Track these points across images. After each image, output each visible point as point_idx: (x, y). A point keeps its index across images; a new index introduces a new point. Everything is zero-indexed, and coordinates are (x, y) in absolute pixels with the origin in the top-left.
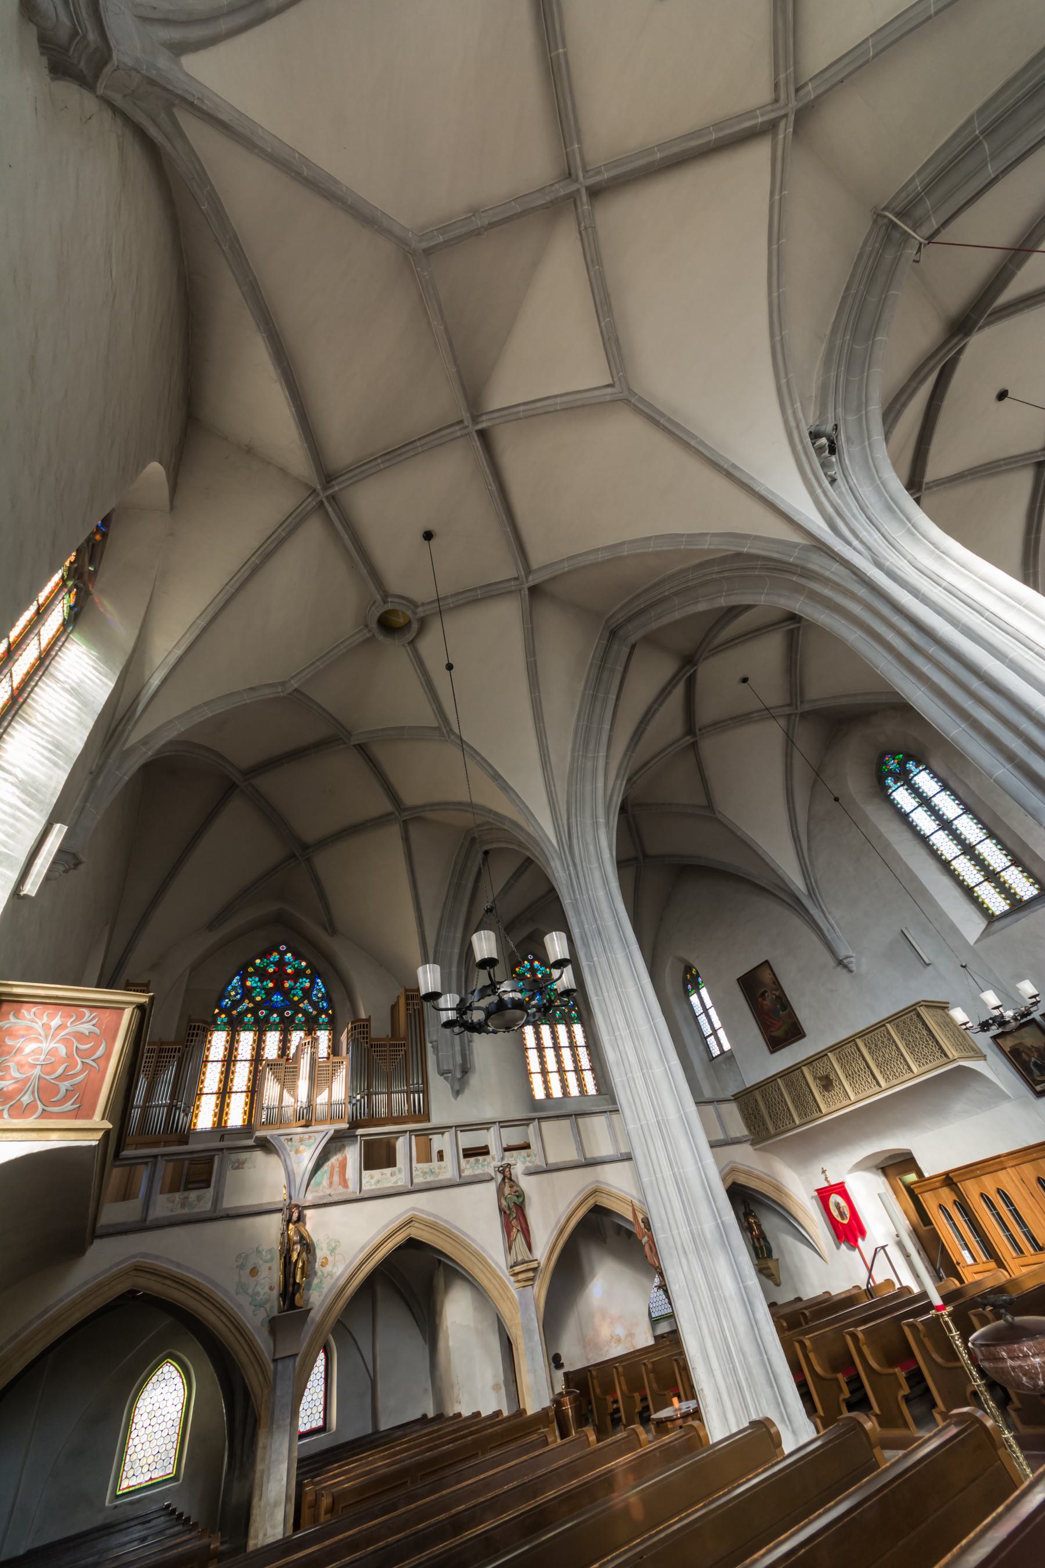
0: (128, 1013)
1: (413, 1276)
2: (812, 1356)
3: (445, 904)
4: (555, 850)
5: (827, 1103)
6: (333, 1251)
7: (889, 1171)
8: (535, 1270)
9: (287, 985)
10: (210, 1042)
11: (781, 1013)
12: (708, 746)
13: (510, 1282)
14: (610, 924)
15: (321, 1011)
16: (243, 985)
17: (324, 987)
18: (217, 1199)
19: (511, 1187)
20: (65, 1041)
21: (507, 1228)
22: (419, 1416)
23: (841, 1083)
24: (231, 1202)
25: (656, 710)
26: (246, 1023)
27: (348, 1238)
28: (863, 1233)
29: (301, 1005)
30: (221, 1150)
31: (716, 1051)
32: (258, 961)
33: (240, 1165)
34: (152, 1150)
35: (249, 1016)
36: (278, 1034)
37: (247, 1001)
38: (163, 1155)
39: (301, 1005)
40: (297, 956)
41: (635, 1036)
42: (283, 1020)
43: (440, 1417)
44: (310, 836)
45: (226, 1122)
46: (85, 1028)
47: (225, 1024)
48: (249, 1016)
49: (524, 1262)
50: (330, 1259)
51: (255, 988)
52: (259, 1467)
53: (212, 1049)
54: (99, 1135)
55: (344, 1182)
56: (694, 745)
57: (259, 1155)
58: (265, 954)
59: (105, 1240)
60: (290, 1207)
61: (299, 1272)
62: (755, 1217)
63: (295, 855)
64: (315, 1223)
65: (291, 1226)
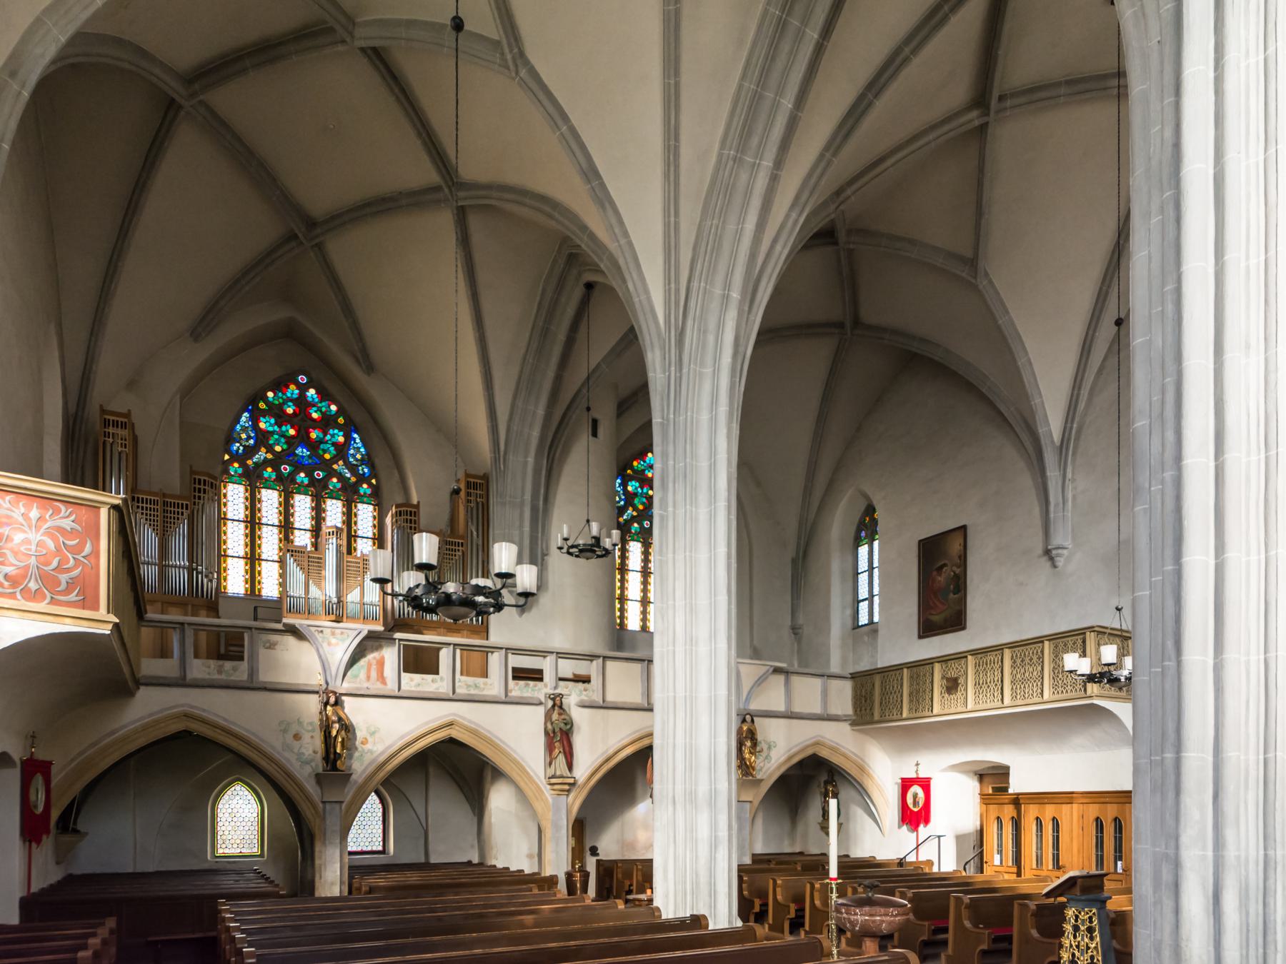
0: (104, 512)
1: (455, 768)
2: (778, 890)
3: (524, 359)
4: (659, 334)
5: (943, 705)
6: (372, 734)
7: (986, 780)
8: (573, 785)
9: (314, 435)
10: (225, 496)
11: (951, 595)
12: (1012, 136)
13: (546, 790)
14: (704, 464)
15: (362, 479)
16: (255, 426)
17: (364, 445)
18: (253, 672)
19: (560, 714)
20: (48, 533)
21: (550, 748)
22: (465, 860)
23: (966, 690)
24: (265, 677)
25: (906, 60)
26: (266, 479)
27: (389, 722)
28: (927, 821)
29: (335, 466)
30: (250, 628)
31: (863, 620)
32: (270, 394)
33: (272, 646)
34: (177, 618)
35: (269, 470)
36: (308, 499)
37: (263, 449)
38: (189, 624)
39: (335, 466)
40: (324, 395)
41: (692, 610)
42: (313, 482)
43: (481, 864)
44: (320, 201)
45: (260, 590)
46: (67, 524)
47: (240, 475)
48: (269, 470)
49: (562, 777)
50: (370, 740)
51: (272, 433)
52: (317, 862)
53: (229, 504)
54: (110, 626)
55: (382, 678)
56: (983, 128)
57: (290, 640)
58: (280, 386)
59: (150, 688)
60: (326, 692)
61: (339, 746)
62: (835, 786)
63: (295, 237)
64: (354, 710)
65: (329, 708)
